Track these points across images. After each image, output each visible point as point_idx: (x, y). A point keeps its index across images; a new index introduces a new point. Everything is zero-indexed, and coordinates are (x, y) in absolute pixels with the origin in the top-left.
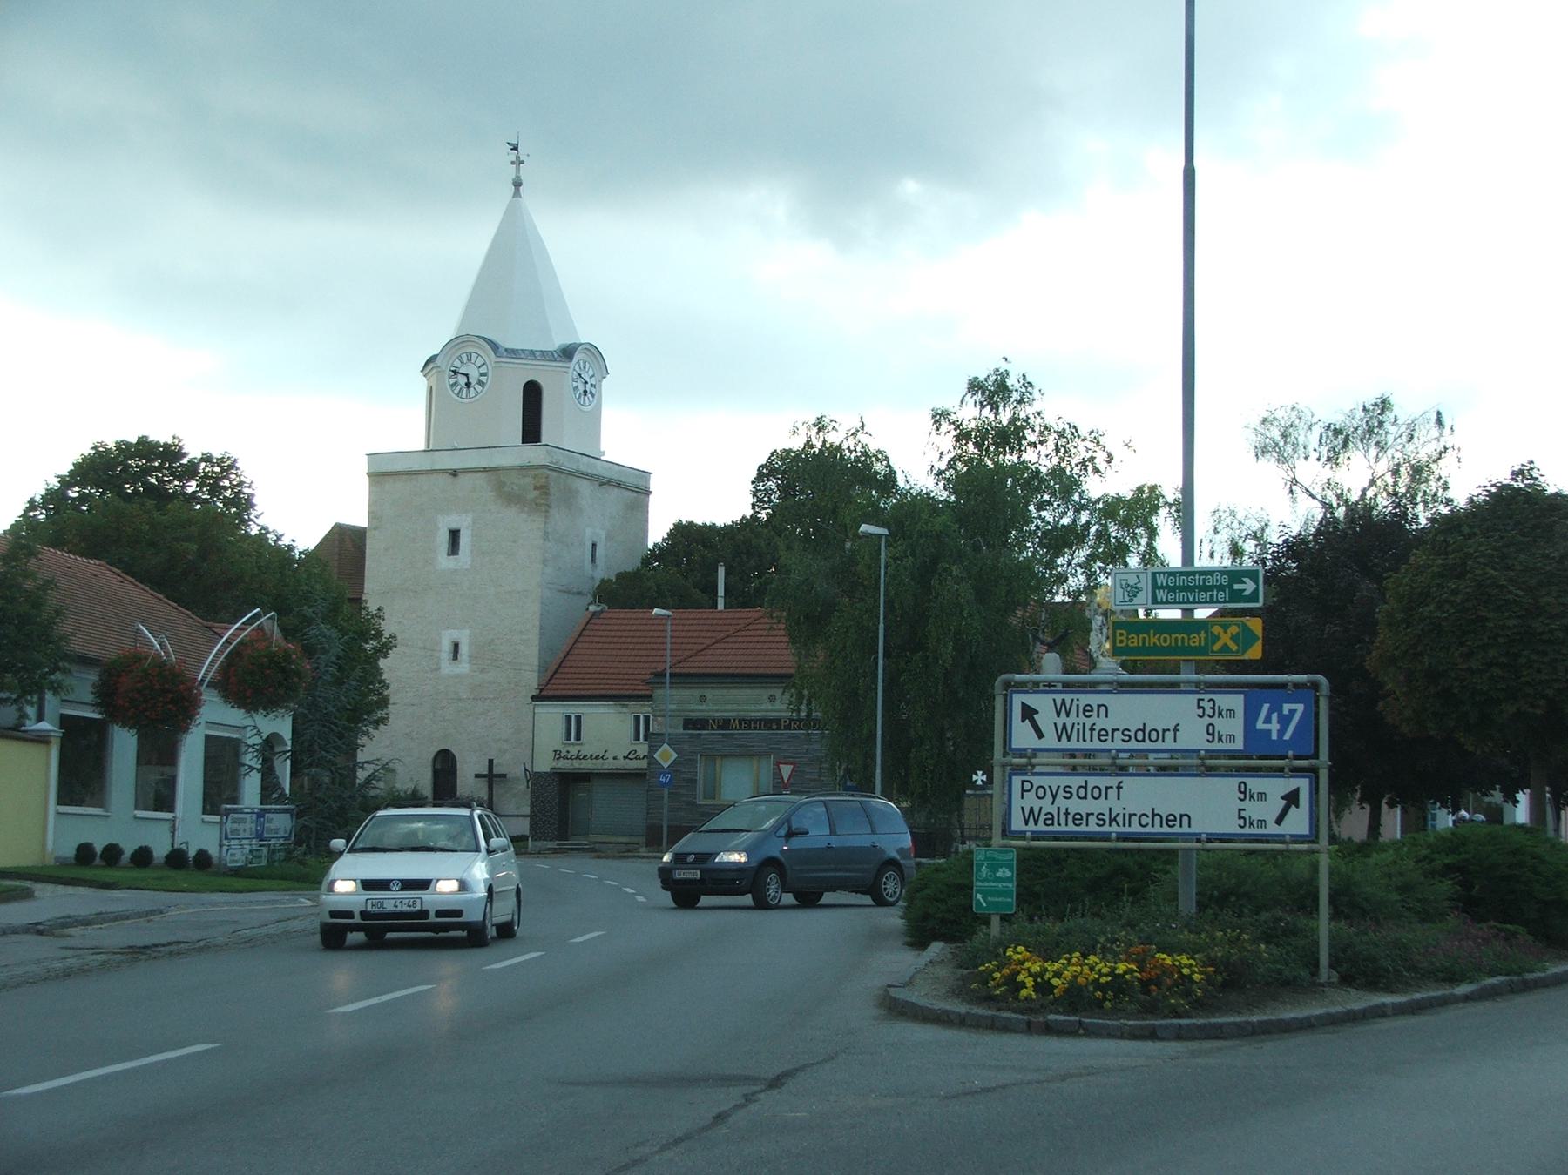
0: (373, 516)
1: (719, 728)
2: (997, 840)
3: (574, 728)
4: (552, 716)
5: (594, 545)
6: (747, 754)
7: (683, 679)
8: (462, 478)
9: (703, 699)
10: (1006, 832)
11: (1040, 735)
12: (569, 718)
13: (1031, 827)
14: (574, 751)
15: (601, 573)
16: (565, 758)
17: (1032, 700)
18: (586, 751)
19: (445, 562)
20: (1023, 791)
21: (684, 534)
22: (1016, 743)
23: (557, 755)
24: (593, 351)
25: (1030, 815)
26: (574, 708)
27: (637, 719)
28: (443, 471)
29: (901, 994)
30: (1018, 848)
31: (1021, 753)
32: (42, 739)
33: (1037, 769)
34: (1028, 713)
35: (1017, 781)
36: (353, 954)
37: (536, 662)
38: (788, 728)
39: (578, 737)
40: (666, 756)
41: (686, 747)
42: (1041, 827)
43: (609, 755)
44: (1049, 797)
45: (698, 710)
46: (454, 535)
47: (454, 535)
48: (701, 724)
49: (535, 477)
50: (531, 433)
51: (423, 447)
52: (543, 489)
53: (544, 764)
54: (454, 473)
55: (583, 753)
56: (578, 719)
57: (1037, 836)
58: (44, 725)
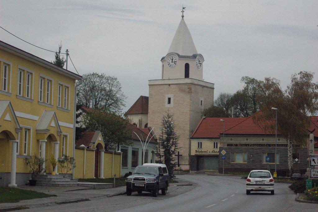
0: (150, 94)
1: (235, 146)
2: (309, 178)
3: (200, 145)
4: (195, 143)
5: (201, 101)
6: (241, 152)
7: (227, 135)
8: (171, 86)
9: (231, 140)
10: (311, 177)
11: (315, 163)
12: (199, 143)
13: (314, 176)
14: (200, 150)
15: (203, 108)
16: (198, 152)
17: (314, 158)
18: (203, 150)
19: (167, 106)
20: (313, 171)
21: (222, 97)
22: (312, 164)
23: (196, 151)
24: (201, 56)
25: (314, 175)
26: (200, 141)
27: (214, 143)
28: (166, 84)
29: (297, 199)
30: (312, 179)
31: (313, 166)
32: (119, 154)
33: (315, 168)
34: (314, 160)
35: (312, 170)
36: (132, 197)
37: (189, 129)
38: (251, 146)
39: (201, 147)
40: (224, 152)
41: (228, 150)
42: (315, 176)
43: (208, 152)
44: (317, 172)
45: (230, 142)
46: (169, 99)
47: (169, 99)
48: (231, 145)
49: (188, 86)
50: (187, 75)
51: (161, 78)
52: (190, 89)
53: (193, 153)
54: (169, 85)
55: (202, 151)
56: (201, 143)
57: (315, 178)
58: (119, 151)
